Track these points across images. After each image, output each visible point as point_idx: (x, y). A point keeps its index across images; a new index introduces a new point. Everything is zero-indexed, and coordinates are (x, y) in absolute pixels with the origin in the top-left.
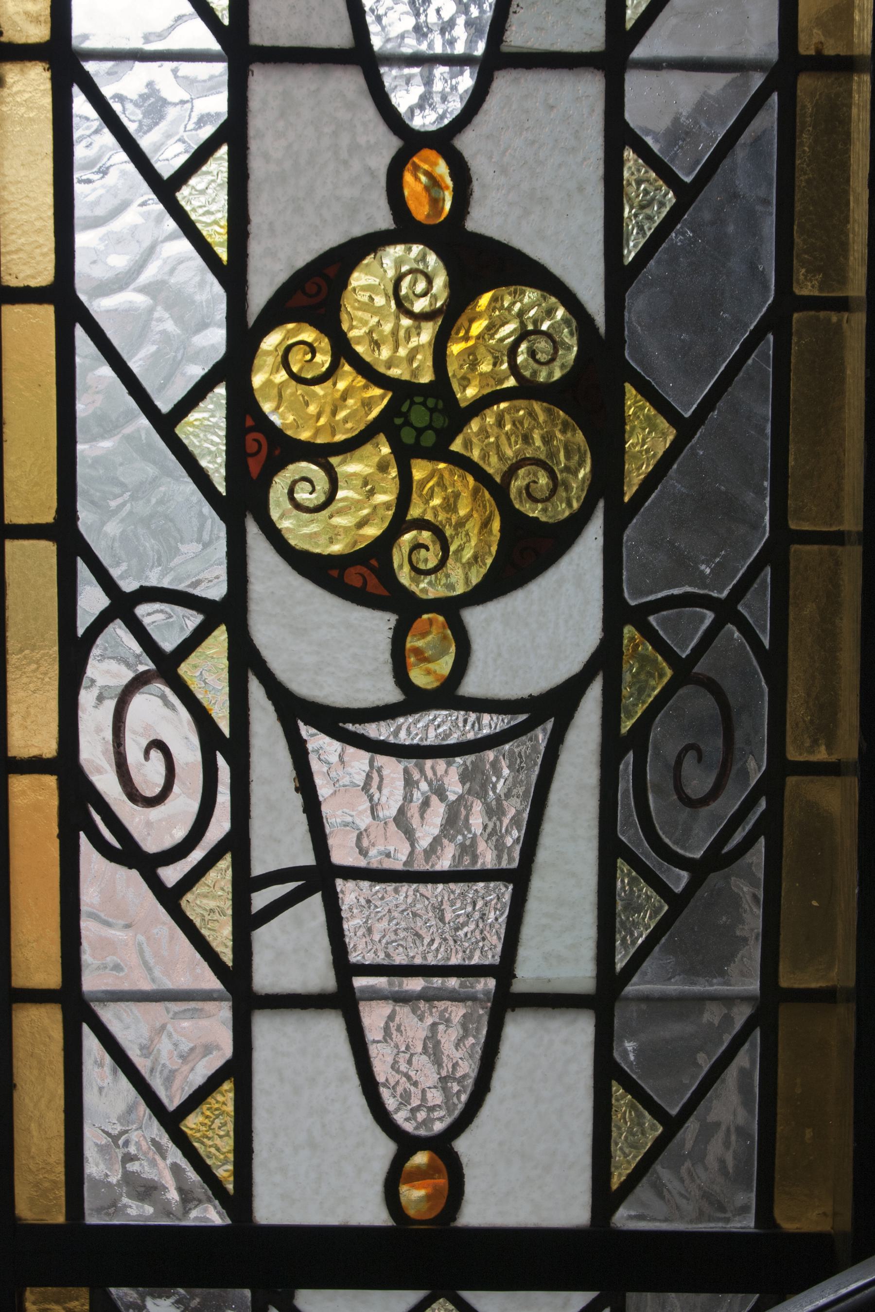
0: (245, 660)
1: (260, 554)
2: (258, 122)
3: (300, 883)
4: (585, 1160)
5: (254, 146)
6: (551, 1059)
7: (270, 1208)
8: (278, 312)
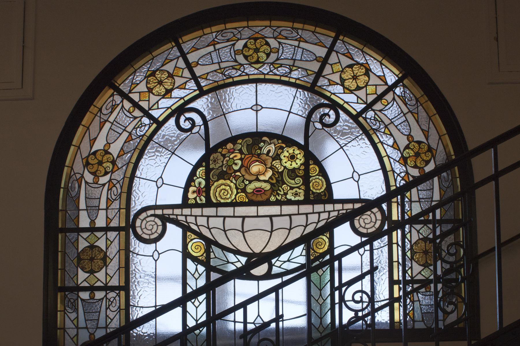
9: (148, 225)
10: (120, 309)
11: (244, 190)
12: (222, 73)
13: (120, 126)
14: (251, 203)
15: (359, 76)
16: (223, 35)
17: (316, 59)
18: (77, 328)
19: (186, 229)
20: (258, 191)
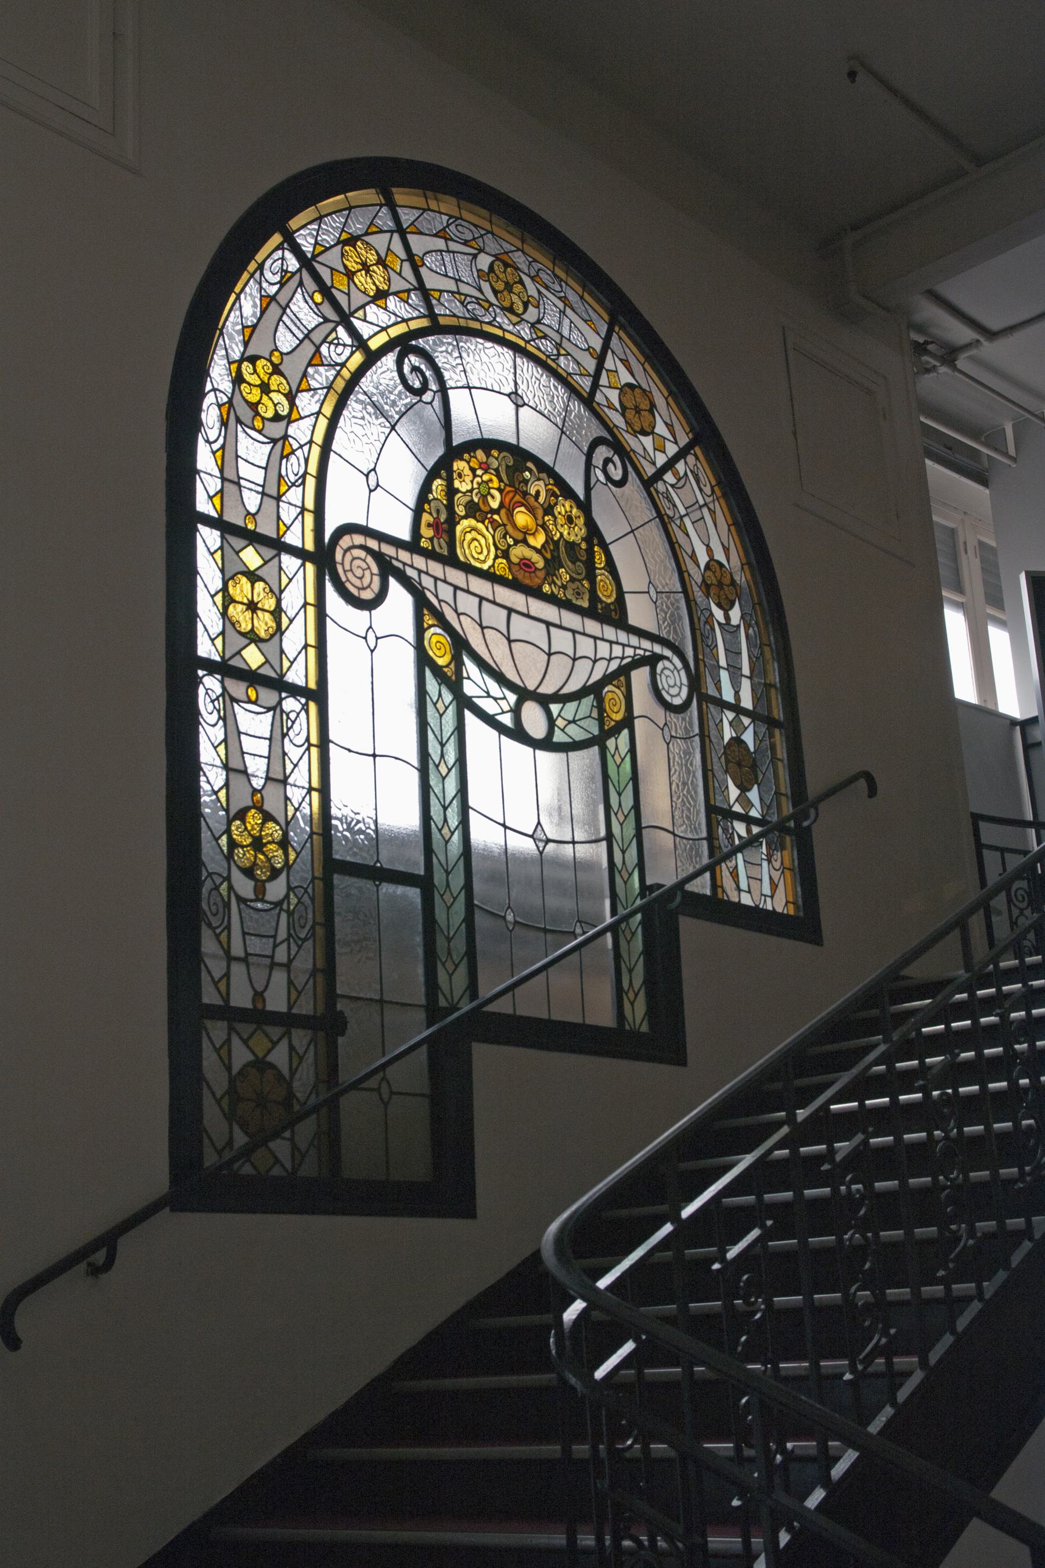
0: (231, 888)
1: (234, 868)
2: (231, 783)
3: (327, 577)
4: (286, 997)
5: (232, 978)
6: (279, 977)
7: (233, 1004)
8: (235, 818)
9: (357, 567)
10: (310, 745)
11: (506, 555)
12: (462, 303)
13: (302, 327)
14: (514, 585)
15: (371, 276)
16: (459, 228)
17: (588, 350)
18: (230, 958)
19: (421, 603)
20: (526, 564)
